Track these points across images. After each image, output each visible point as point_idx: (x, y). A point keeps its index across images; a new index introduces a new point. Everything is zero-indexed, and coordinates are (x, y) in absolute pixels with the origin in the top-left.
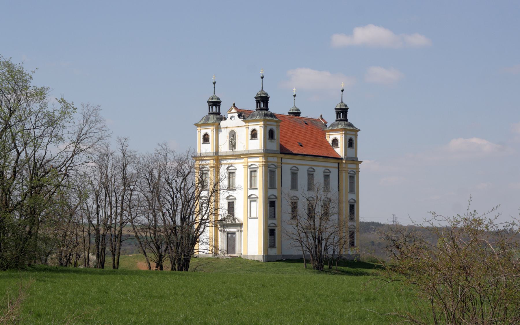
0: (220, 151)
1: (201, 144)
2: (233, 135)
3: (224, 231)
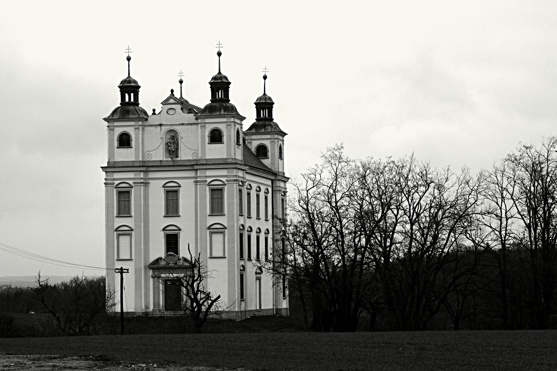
2: (174, 136)
3: (159, 277)
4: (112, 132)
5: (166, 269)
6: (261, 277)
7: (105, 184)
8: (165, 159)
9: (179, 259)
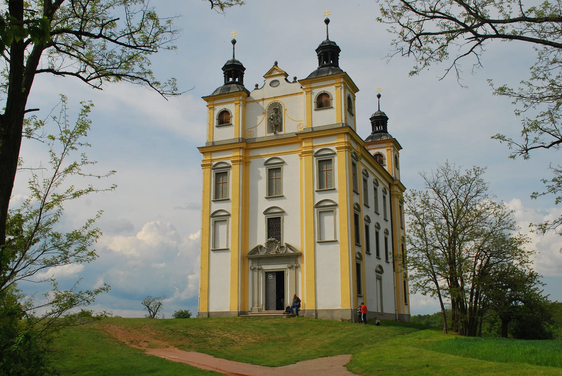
2: (277, 109)
4: (211, 110)
5: (269, 259)
7: (203, 165)
8: (268, 135)
9: (282, 247)
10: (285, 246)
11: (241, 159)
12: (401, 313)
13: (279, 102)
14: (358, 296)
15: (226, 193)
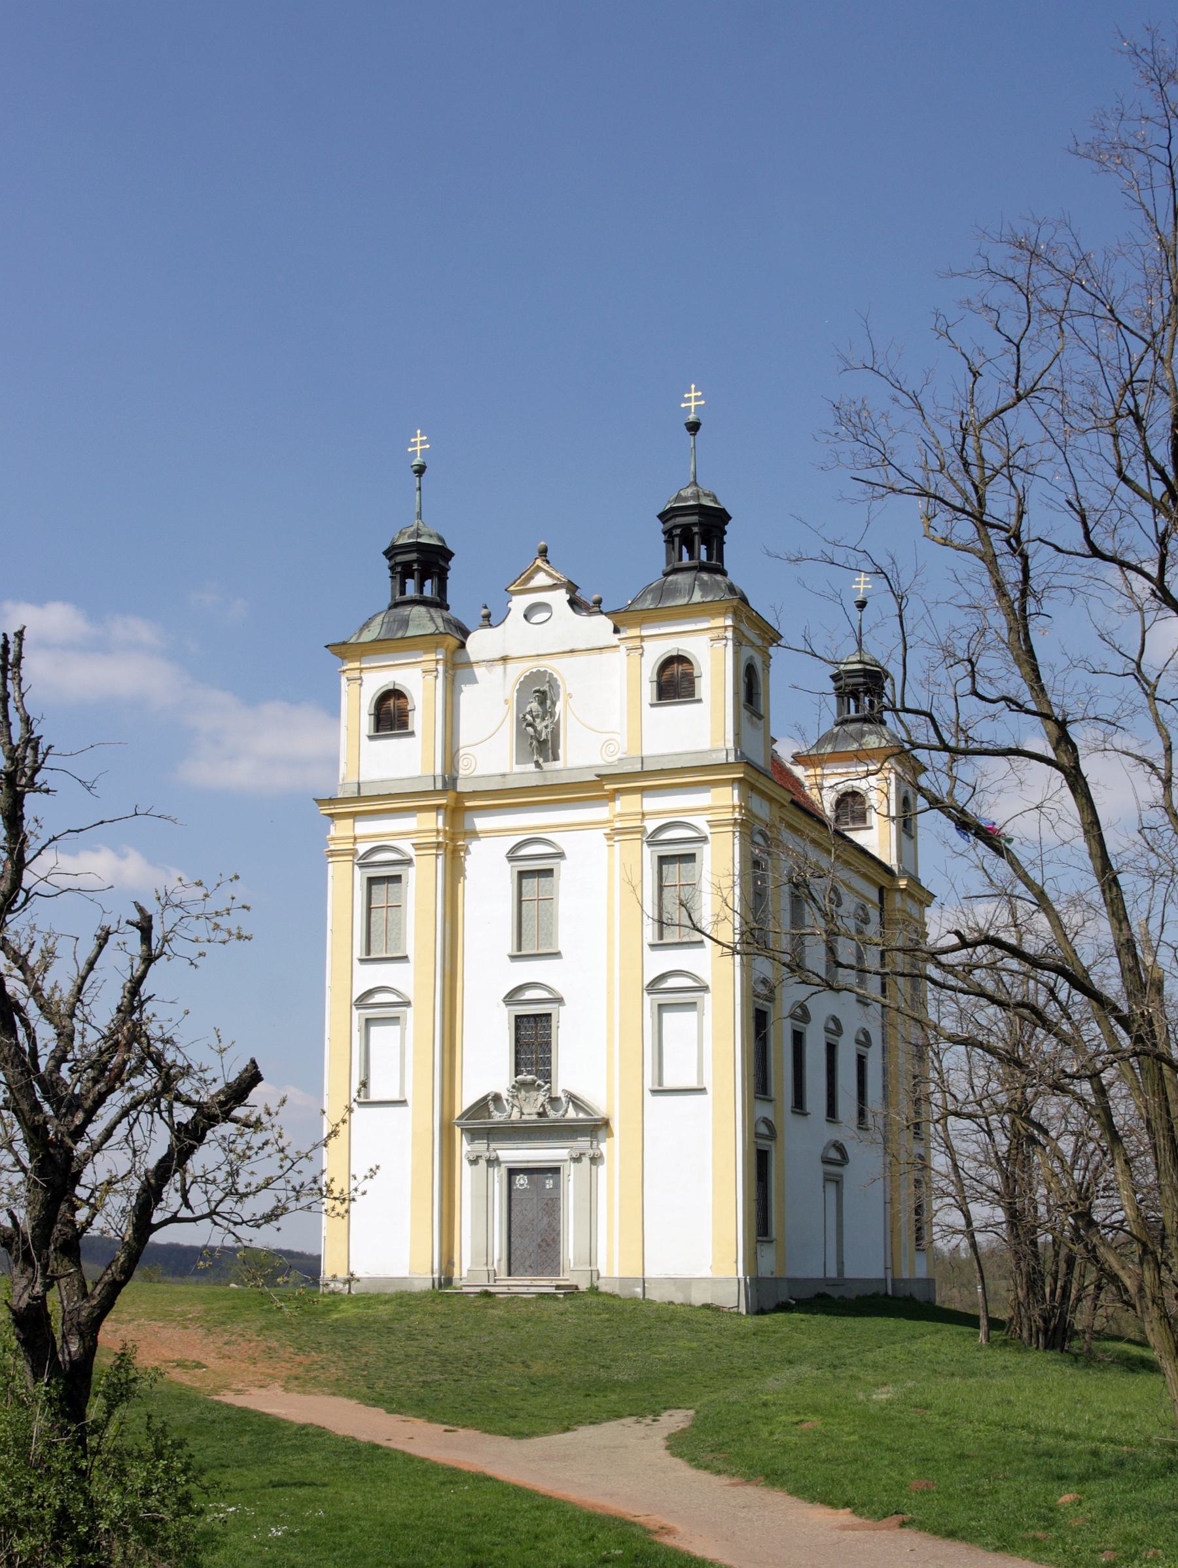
0: (462, 772)
1: (365, 741)
2: (544, 693)
3: (492, 1162)
6: (841, 1176)
8: (518, 769)
9: (553, 1100)
10: (564, 1099)
11: (441, 839)
12: (904, 1277)
13: (550, 671)
14: (758, 1241)
15: (399, 938)
